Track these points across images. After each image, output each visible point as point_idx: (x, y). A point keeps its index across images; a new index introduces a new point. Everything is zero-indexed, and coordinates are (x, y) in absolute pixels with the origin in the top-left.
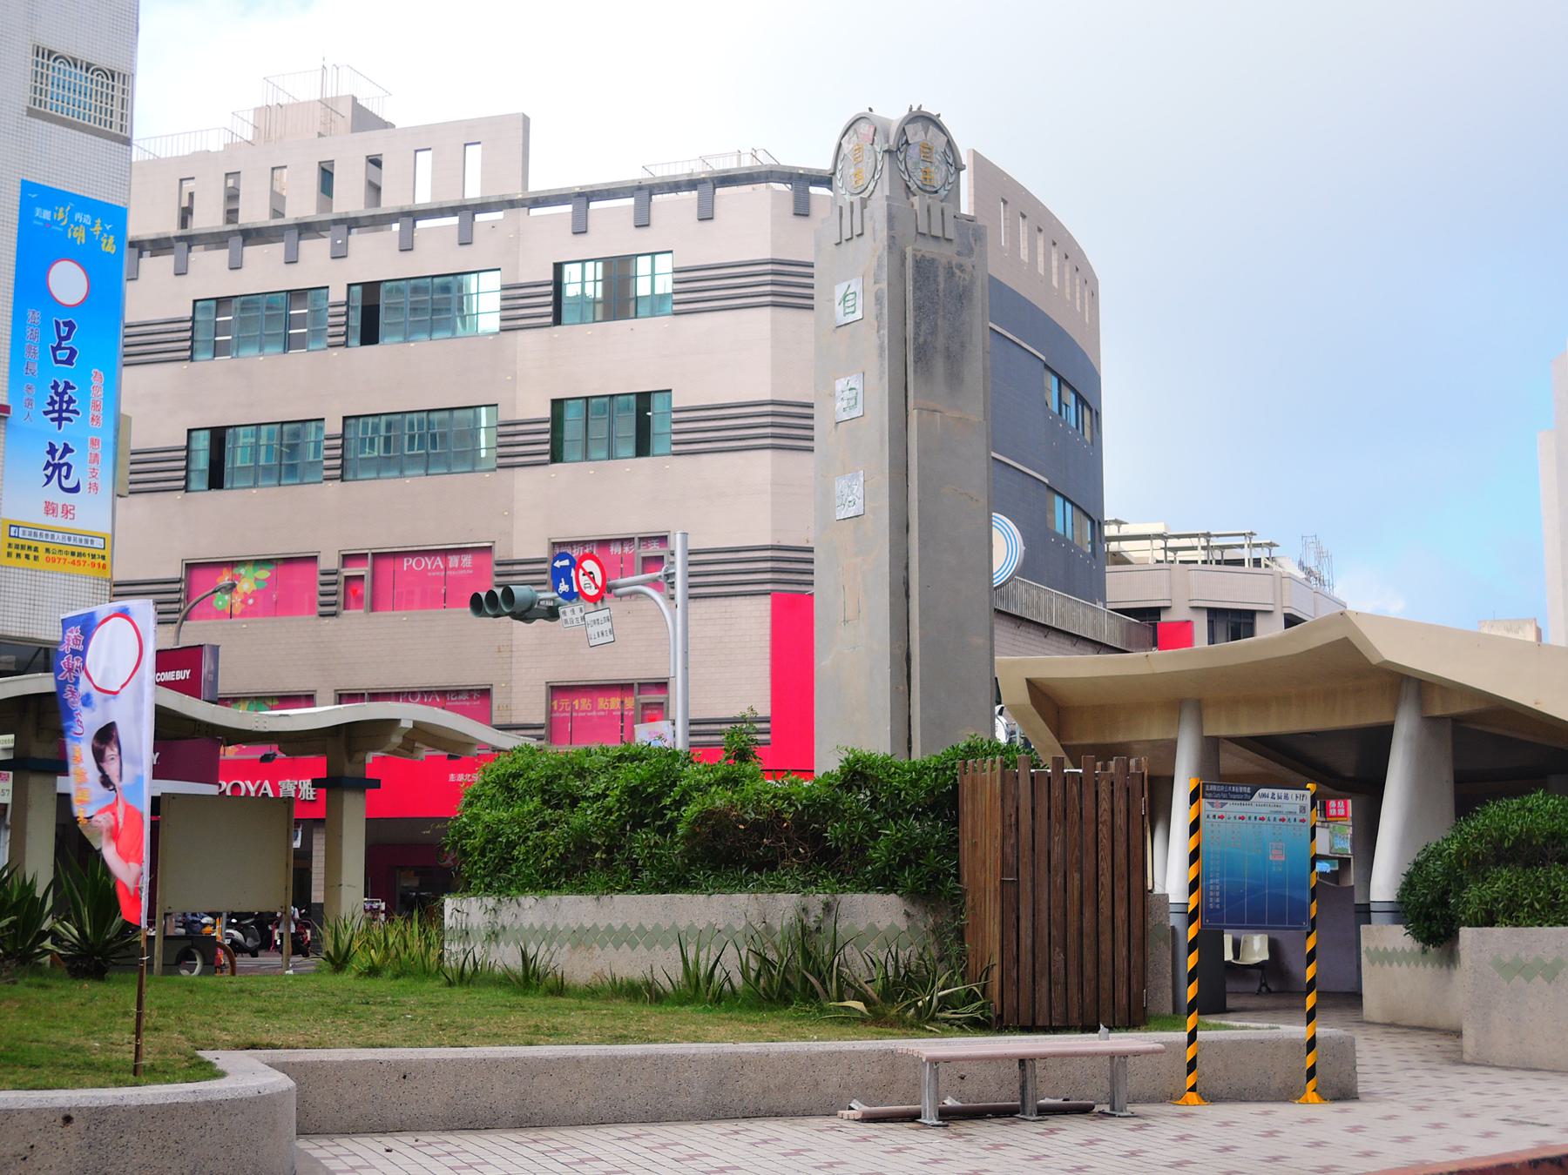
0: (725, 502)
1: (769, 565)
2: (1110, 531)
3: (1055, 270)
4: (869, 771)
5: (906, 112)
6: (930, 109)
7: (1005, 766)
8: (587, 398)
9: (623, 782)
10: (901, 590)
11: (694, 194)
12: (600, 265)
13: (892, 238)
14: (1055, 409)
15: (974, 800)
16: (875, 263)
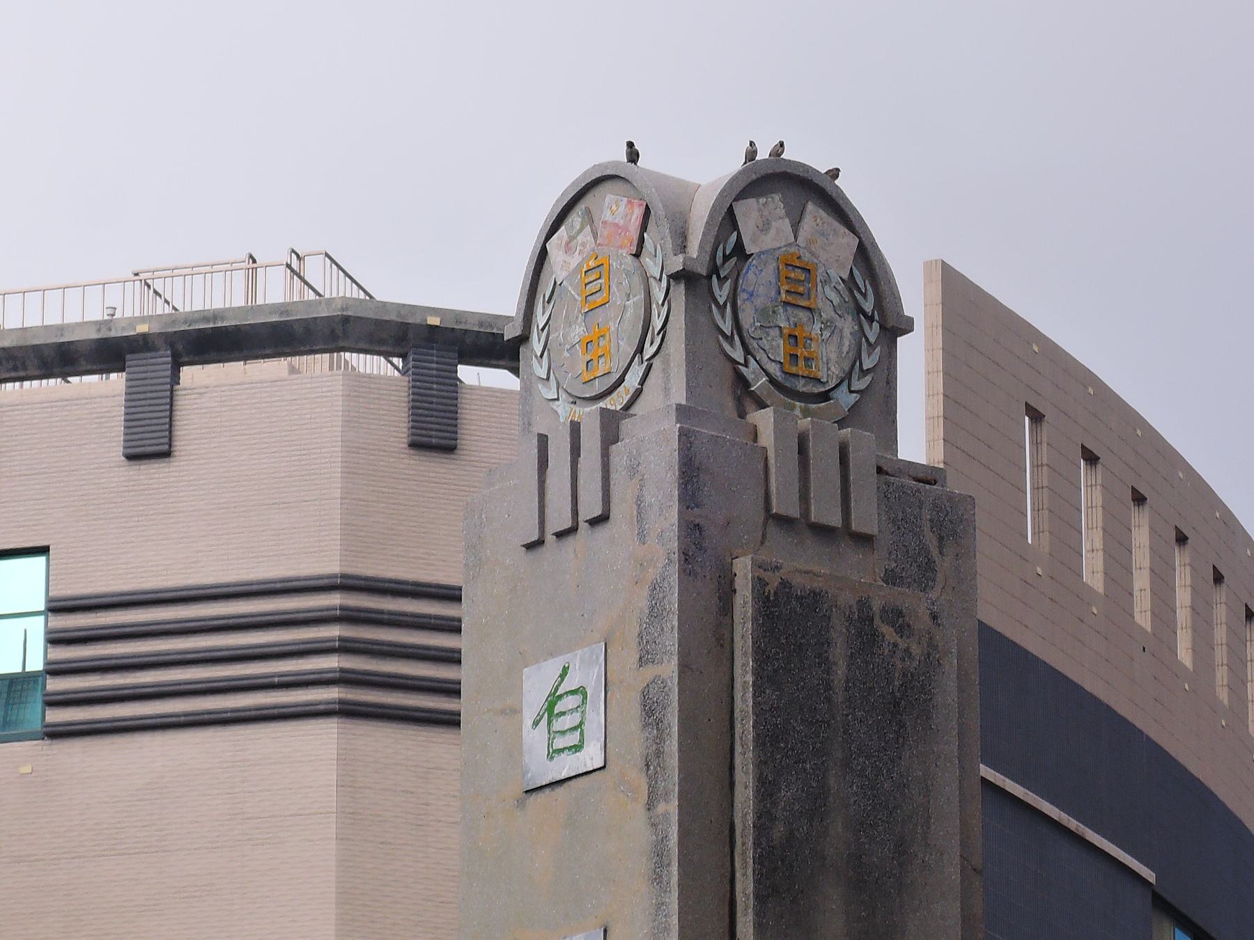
3: (1183, 616)
5: (736, 163)
11: (117, 380)
13: (692, 531)
16: (642, 601)
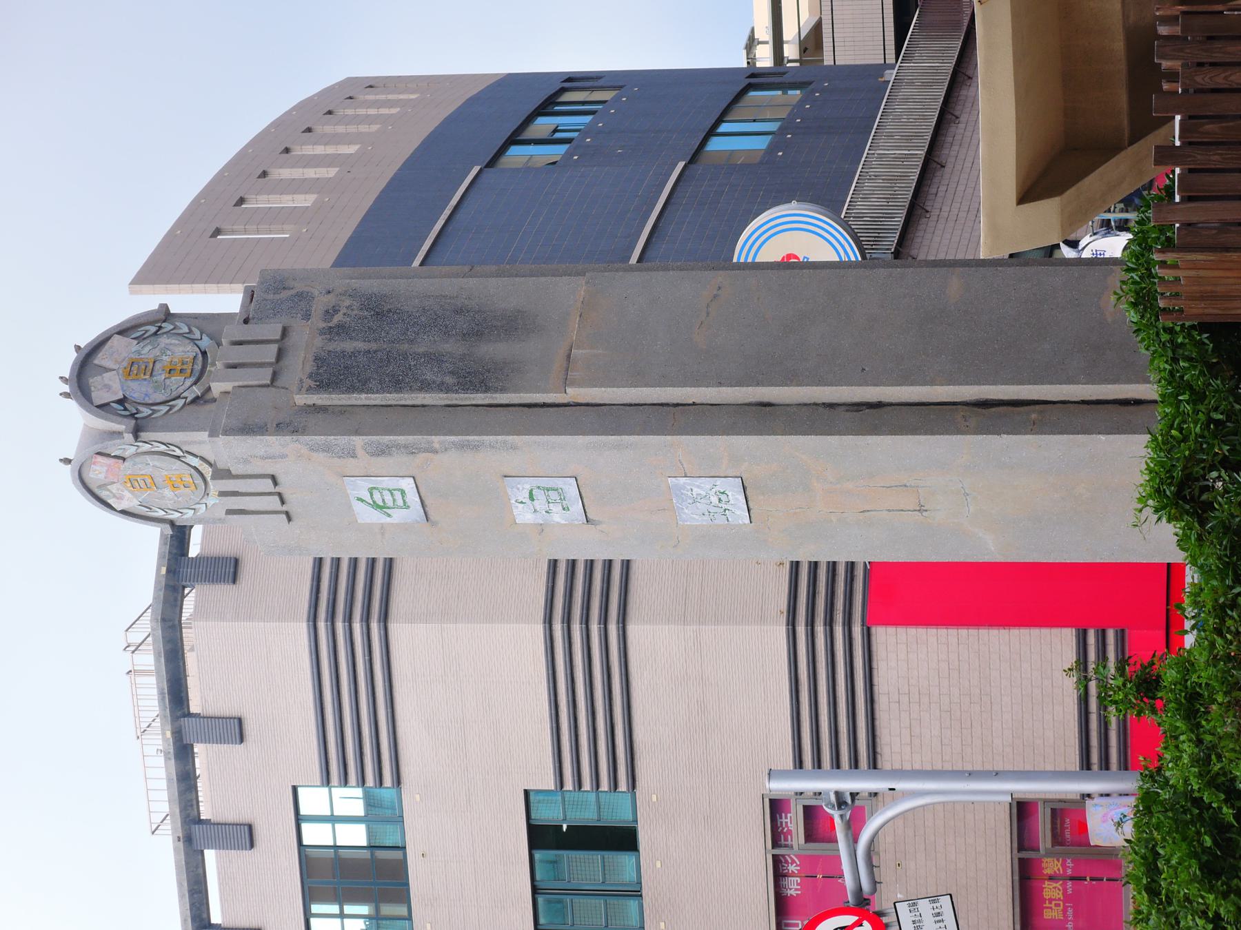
0: (713, 711)
1: (820, 629)
2: (764, 58)
3: (330, 150)
4: (1177, 474)
5: (72, 404)
6: (66, 362)
7: (1169, 245)
8: (535, 890)
9: (1193, 890)
10: (871, 417)
11: (198, 748)
12: (315, 908)
14: (561, 149)
15: (1228, 297)
